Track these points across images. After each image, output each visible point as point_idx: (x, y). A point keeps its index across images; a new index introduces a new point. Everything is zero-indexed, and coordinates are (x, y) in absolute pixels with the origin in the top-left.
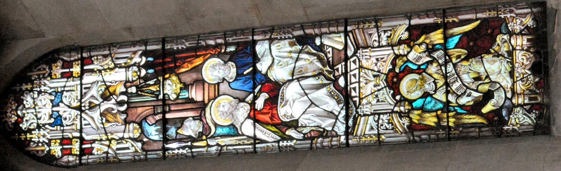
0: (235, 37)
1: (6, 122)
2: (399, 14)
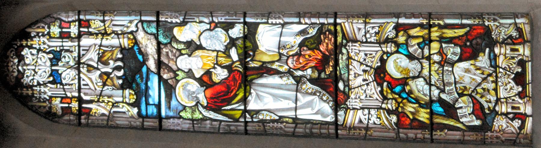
0: (227, 17)
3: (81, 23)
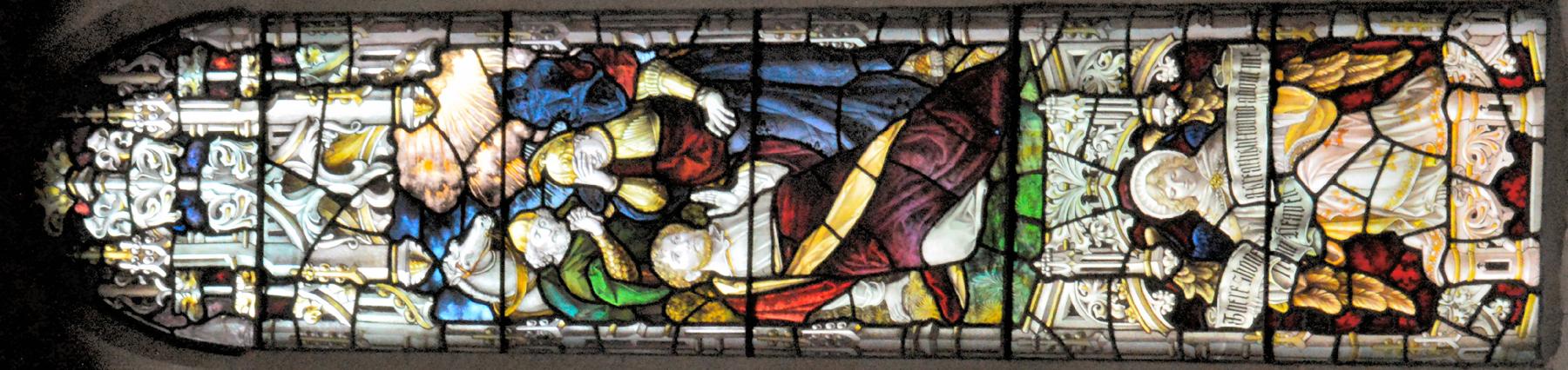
2: (393, 14)
3: (265, 54)
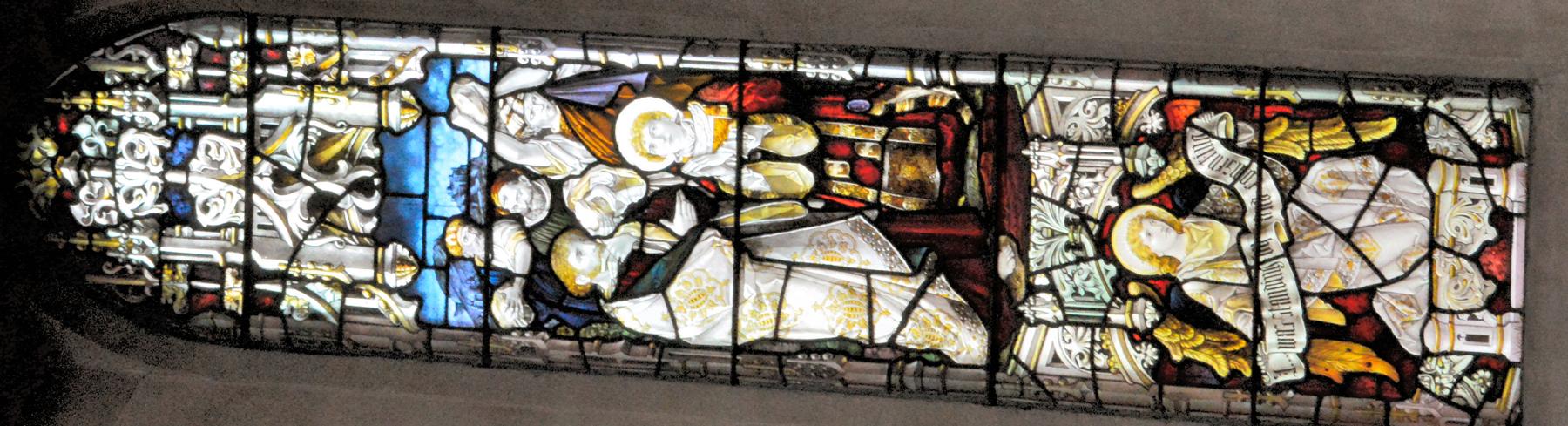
1: (28, 192)
3: (255, 52)
